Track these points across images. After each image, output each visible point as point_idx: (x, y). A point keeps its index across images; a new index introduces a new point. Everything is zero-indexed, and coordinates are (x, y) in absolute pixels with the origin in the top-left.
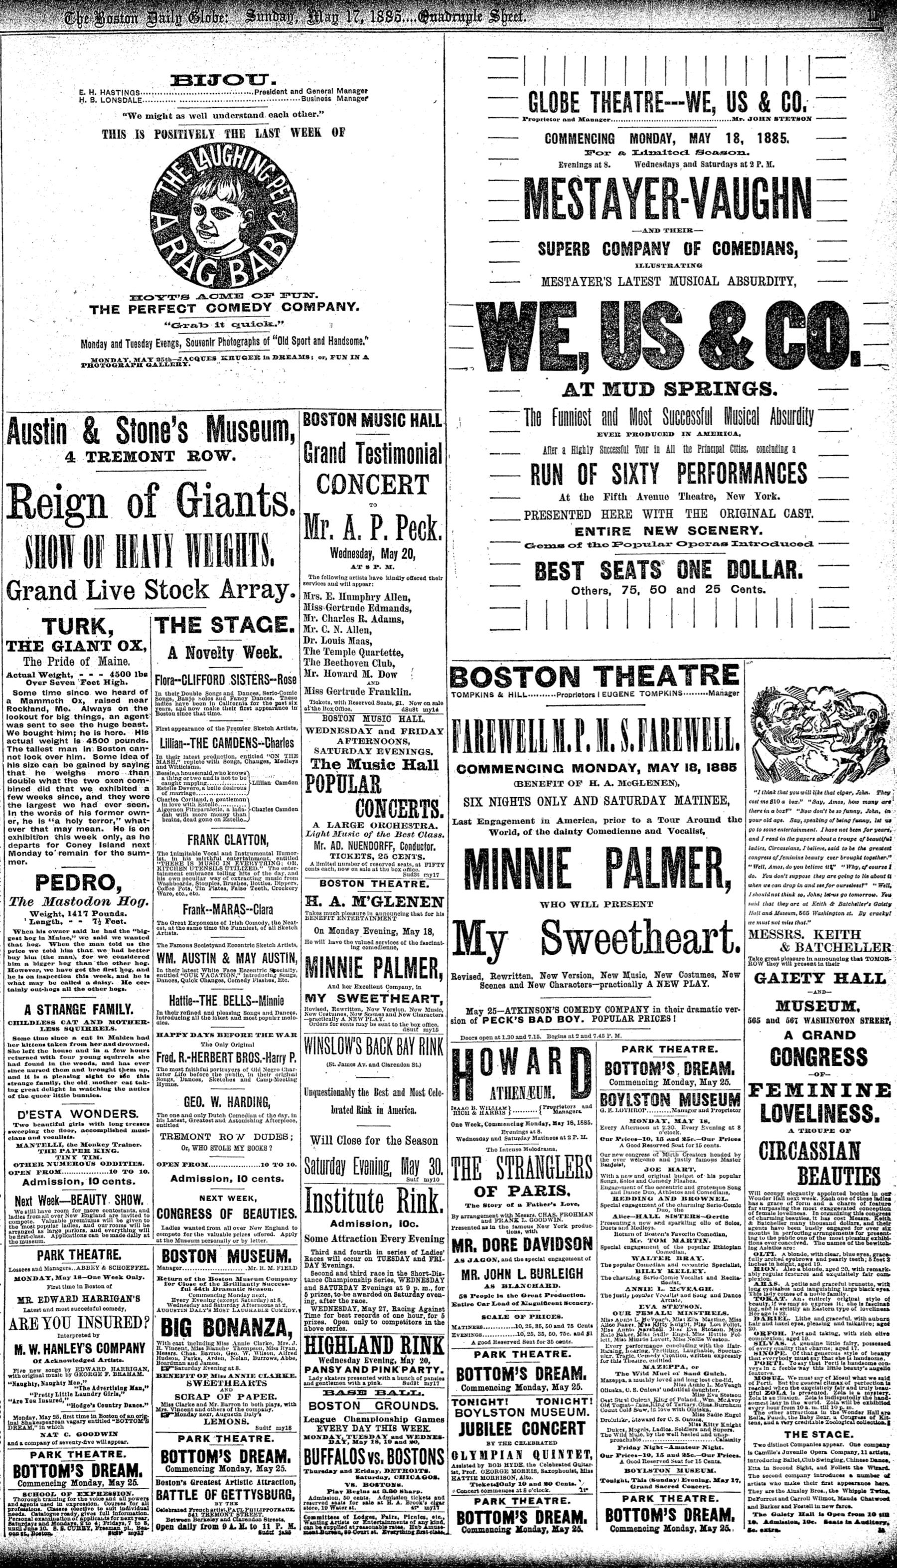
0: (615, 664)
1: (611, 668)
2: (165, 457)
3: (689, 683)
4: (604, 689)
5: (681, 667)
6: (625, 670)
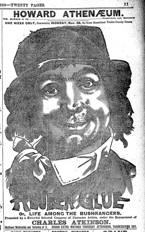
0: (76, 10)
1: (74, 12)
2: (23, 5)
3: (72, 16)
4: (15, 18)
5: (70, 12)
6: (79, 12)
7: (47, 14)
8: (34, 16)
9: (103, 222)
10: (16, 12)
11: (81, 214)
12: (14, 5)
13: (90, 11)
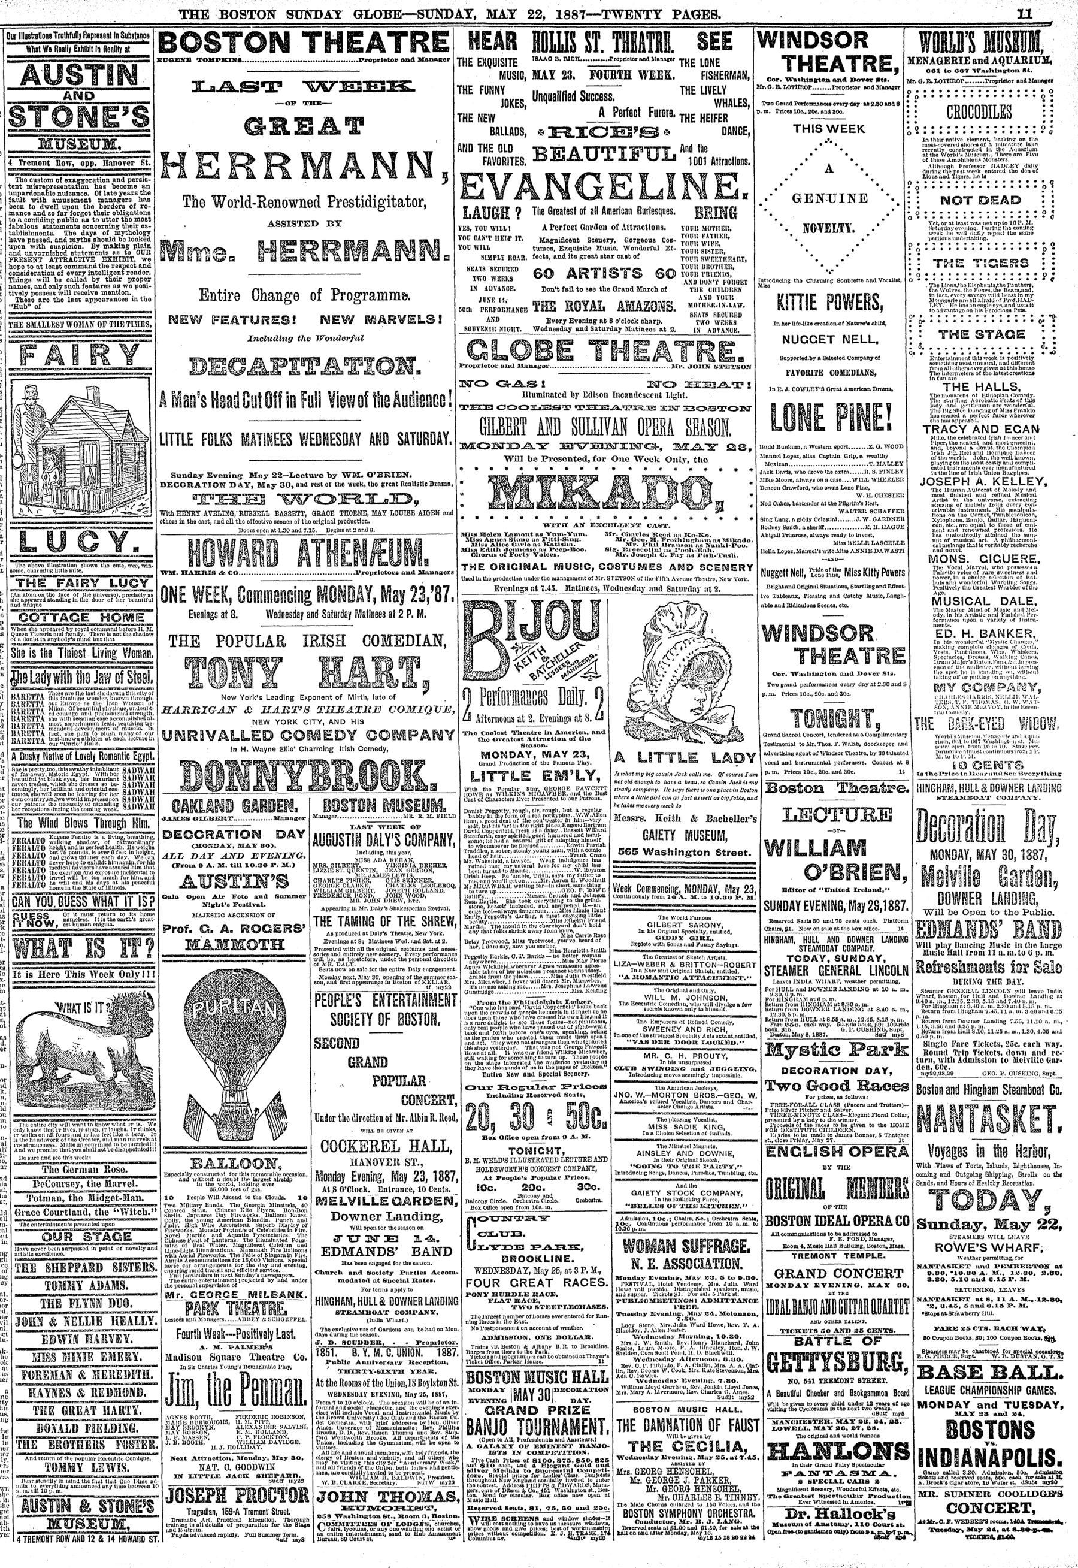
0: (323, 30)
1: (319, 34)
3: (854, 69)
7: (422, 42)
12: (611, 16)
13: (790, 34)
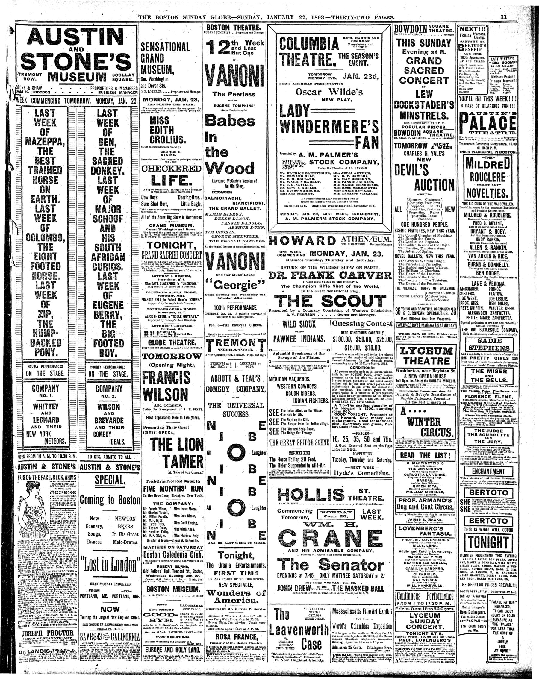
8: (300, 244)
9: (369, 567)
10: (273, 238)
11: (250, 492)
